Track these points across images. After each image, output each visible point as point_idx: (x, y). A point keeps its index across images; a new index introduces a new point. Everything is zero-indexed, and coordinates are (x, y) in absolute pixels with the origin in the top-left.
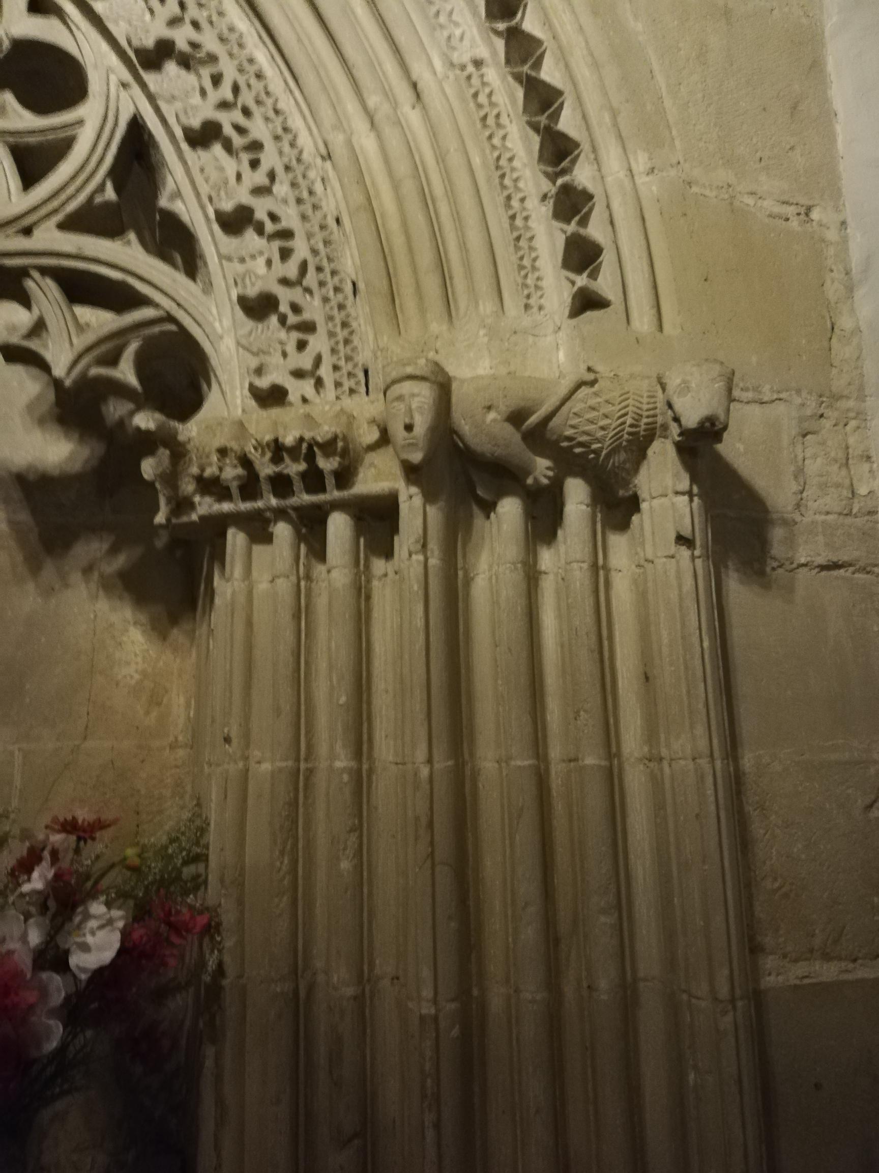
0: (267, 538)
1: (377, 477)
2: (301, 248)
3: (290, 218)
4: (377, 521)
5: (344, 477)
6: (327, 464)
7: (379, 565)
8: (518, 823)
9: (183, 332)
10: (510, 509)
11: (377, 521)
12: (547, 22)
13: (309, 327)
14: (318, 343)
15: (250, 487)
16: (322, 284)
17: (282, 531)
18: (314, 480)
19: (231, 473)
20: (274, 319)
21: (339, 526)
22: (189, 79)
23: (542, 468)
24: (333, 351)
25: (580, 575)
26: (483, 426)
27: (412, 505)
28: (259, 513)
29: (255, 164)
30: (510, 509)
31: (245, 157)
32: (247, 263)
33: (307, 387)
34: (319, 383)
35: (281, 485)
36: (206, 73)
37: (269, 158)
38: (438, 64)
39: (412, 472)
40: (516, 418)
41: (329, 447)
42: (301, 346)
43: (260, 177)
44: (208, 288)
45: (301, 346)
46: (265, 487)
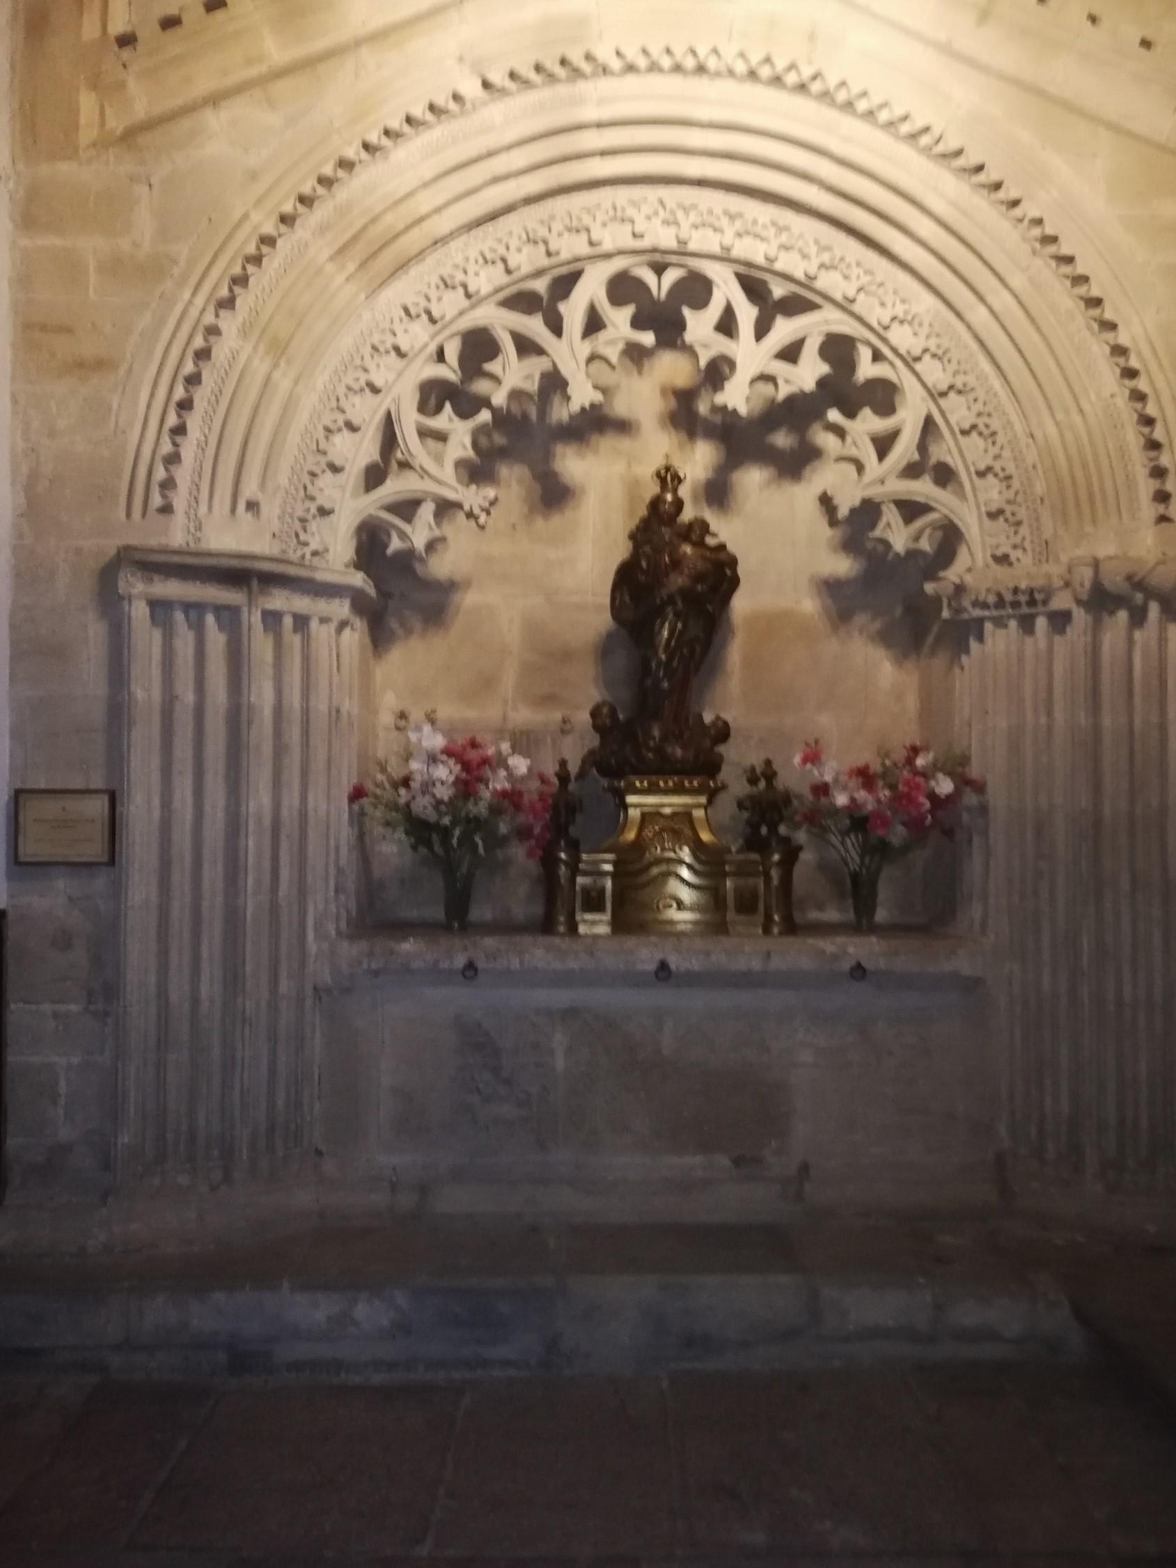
0: (1006, 626)
1: (1061, 601)
2: (1016, 483)
3: (1011, 469)
4: (1060, 620)
5: (1045, 602)
6: (1038, 597)
7: (1057, 638)
8: (250, 613)
9: (951, 522)
10: (1123, 616)
11: (1060, 620)
12: (1152, 382)
13: (1019, 523)
14: (1024, 530)
15: (1001, 603)
16: (1026, 501)
17: (1013, 624)
18: (1032, 602)
19: (991, 599)
20: (1001, 519)
21: (1041, 623)
22: (961, 399)
23: (1139, 597)
24: (1032, 534)
25: (1153, 643)
26: (1114, 580)
27: (1080, 617)
28: (1001, 617)
29: (994, 443)
30: (1123, 616)
31: (990, 441)
32: (993, 493)
33: (1019, 553)
34: (1024, 550)
35: (1015, 605)
36: (971, 396)
37: (1000, 439)
38: (1093, 397)
39: (1079, 602)
40: (1129, 578)
41: (1041, 590)
42: (1016, 533)
43: (996, 450)
44: (962, 496)
45: (1016, 533)
46: (1008, 606)
